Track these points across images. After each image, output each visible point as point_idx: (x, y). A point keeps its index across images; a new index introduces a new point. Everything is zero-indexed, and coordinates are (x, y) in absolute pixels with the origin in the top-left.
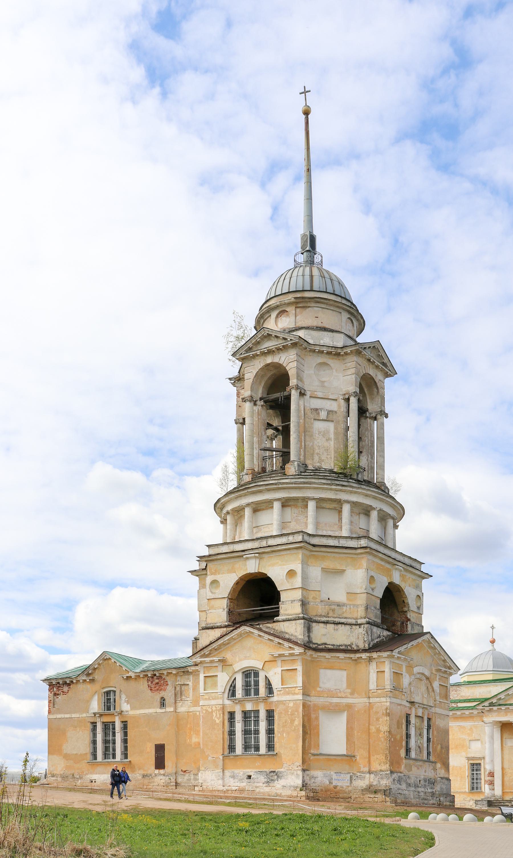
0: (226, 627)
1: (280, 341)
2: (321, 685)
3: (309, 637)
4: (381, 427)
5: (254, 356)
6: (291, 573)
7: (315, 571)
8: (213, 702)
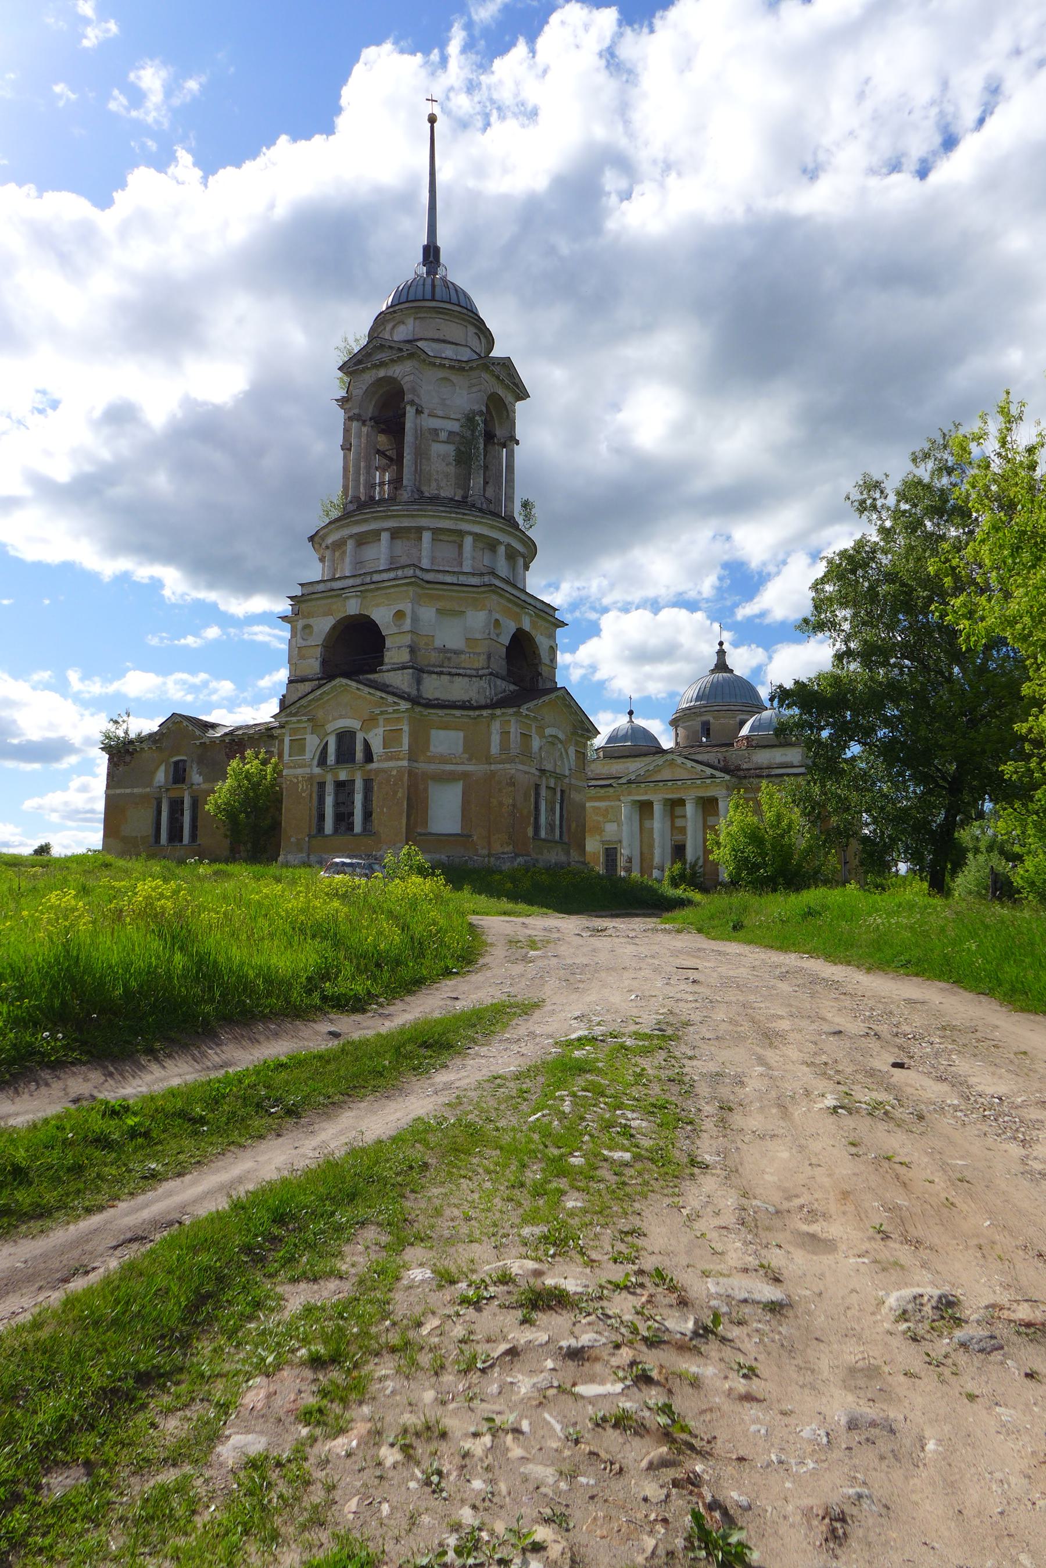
0: (319, 679)
2: (432, 748)
3: (418, 690)
4: (511, 455)
5: (364, 370)
6: (400, 615)
8: (299, 771)
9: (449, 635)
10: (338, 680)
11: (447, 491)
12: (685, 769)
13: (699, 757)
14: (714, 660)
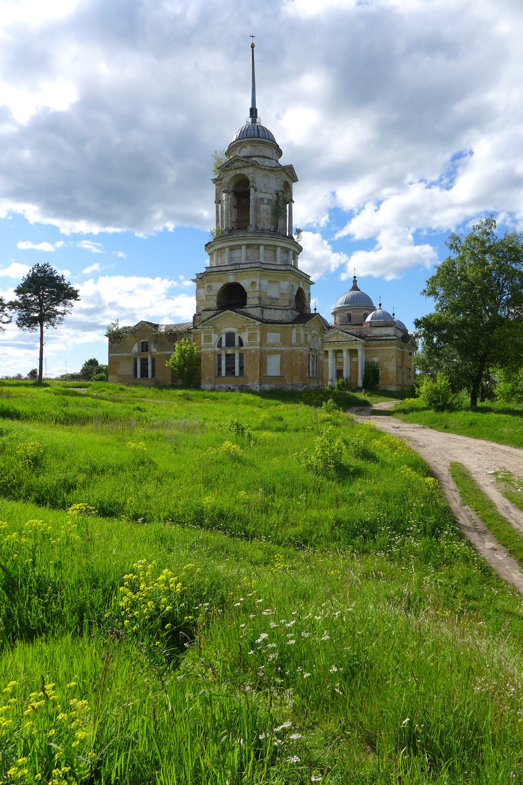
1: (244, 163)
6: (253, 283)
7: (265, 282)
8: (209, 349)
9: (273, 292)
10: (227, 311)
11: (268, 226)
12: (343, 337)
13: (348, 331)
14: (352, 285)
